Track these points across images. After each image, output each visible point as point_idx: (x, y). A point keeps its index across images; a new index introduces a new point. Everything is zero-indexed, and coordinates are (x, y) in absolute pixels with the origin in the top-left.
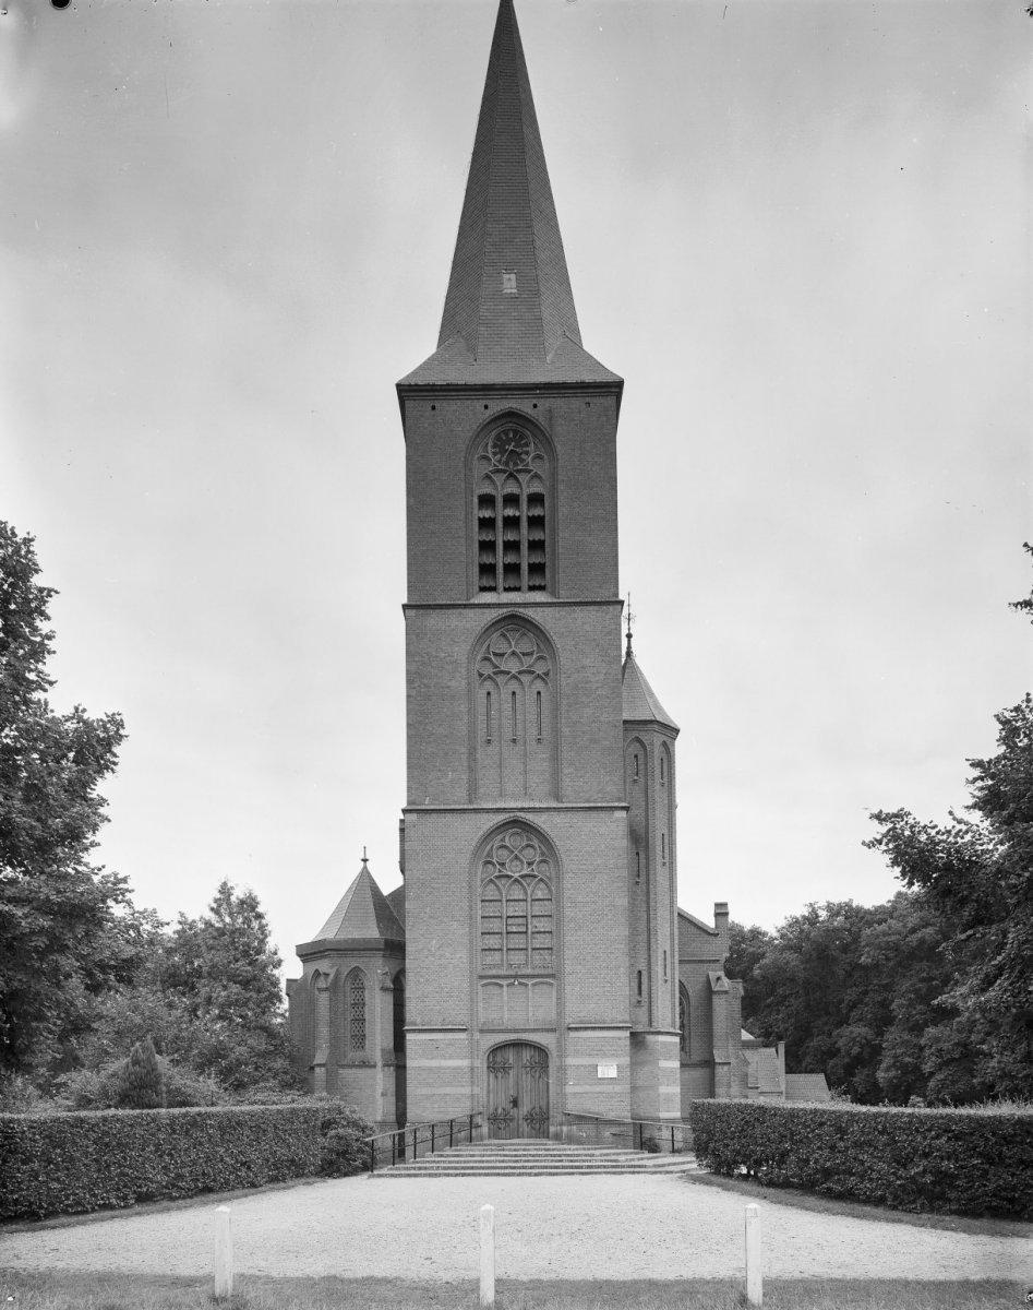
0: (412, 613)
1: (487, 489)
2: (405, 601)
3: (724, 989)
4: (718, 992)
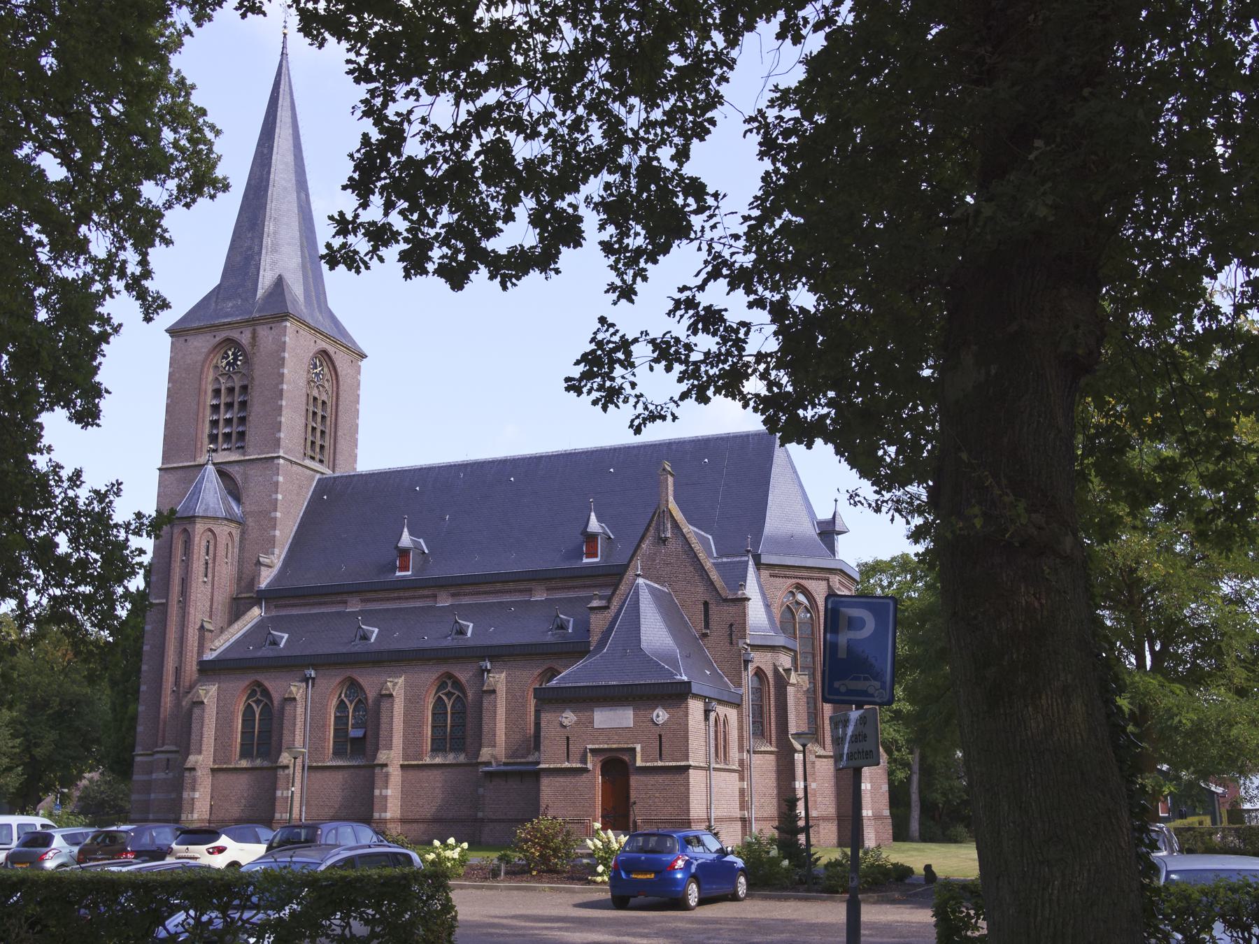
2: (160, 465)
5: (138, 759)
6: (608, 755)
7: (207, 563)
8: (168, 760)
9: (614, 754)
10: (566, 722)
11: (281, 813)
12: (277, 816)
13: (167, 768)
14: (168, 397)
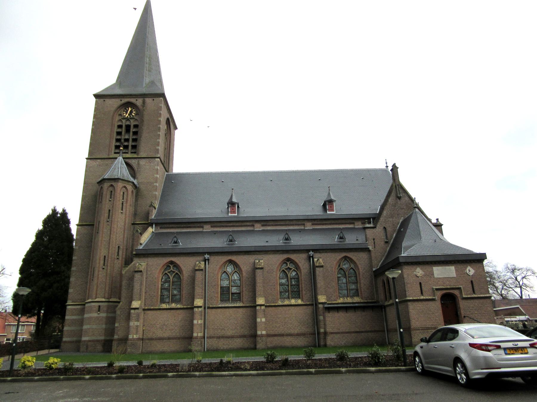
0: (89, 160)
1: (120, 123)
2: (87, 157)
3: (321, 265)
4: (317, 267)
5: (68, 307)
6: (445, 292)
7: (123, 204)
8: (99, 306)
9: (448, 291)
10: (419, 275)
11: (198, 333)
12: (195, 335)
13: (99, 311)
14: (93, 125)
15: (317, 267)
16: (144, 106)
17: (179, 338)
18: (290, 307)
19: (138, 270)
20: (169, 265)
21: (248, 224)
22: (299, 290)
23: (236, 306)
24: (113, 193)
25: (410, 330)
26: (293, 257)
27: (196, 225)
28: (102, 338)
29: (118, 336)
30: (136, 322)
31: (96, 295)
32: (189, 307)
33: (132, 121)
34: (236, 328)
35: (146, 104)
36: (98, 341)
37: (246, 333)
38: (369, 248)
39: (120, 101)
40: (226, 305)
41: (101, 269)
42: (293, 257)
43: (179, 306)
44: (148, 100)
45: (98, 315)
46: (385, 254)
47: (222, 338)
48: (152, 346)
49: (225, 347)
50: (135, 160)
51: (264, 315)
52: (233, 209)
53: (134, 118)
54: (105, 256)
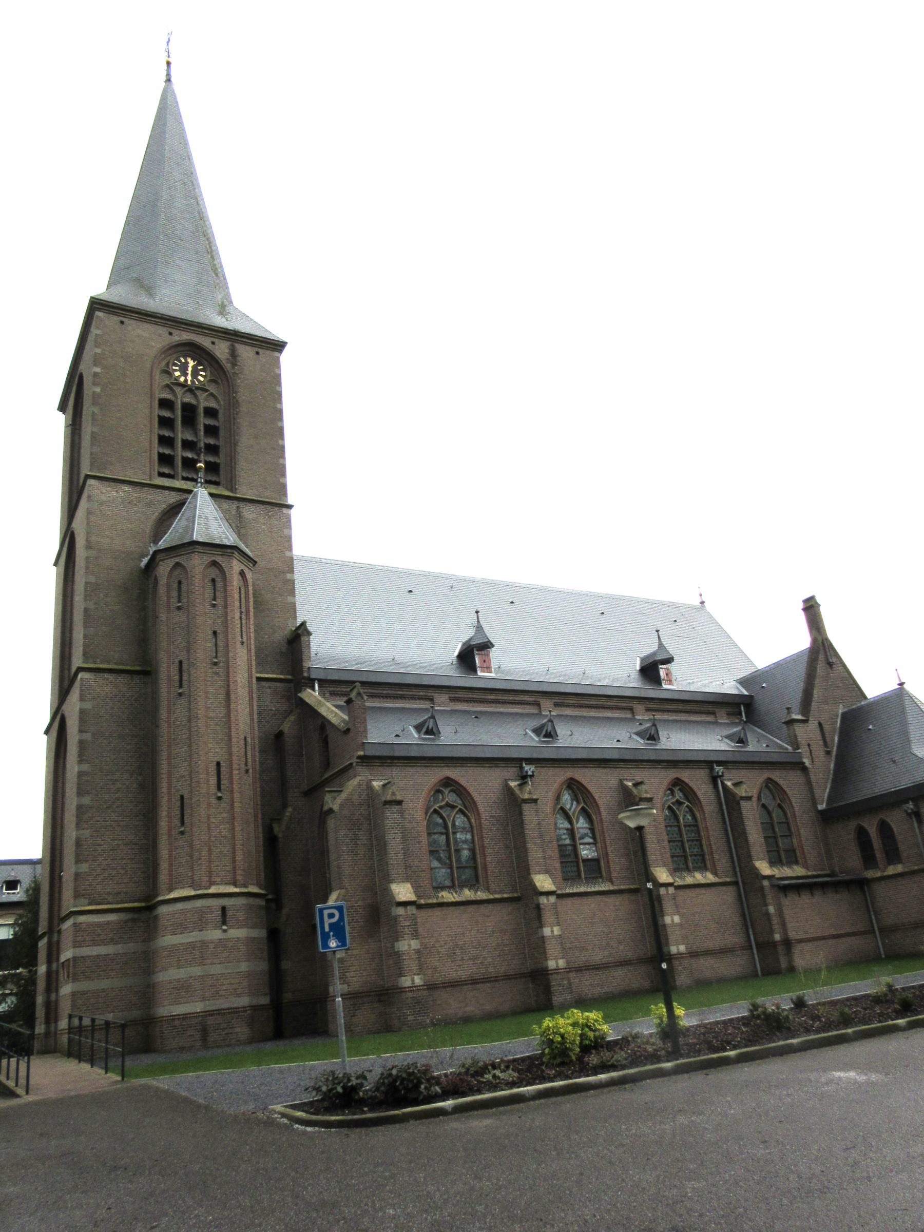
1: (167, 395)
8: (224, 909)
13: (224, 923)
15: (743, 800)
16: (237, 365)
17: (508, 977)
18: (698, 890)
19: (394, 798)
20: (441, 788)
21: (527, 698)
22: (702, 850)
23: (571, 891)
24: (219, 585)
25: (548, 974)
26: (685, 775)
27: (415, 692)
28: (244, 1001)
29: (349, 986)
30: (413, 939)
31: (210, 874)
32: (505, 896)
33: (202, 396)
34: (608, 944)
35: (239, 358)
36: (234, 1011)
37: (630, 955)
38: (804, 763)
39: (167, 334)
40: (575, 890)
41: (213, 801)
42: (685, 775)
43: (481, 895)
44: (245, 352)
45: (223, 936)
46: (828, 776)
47: (586, 970)
48: (439, 1005)
49: (597, 991)
50: (230, 502)
51: (677, 907)
52: (484, 661)
53: (206, 391)
54: (218, 764)
